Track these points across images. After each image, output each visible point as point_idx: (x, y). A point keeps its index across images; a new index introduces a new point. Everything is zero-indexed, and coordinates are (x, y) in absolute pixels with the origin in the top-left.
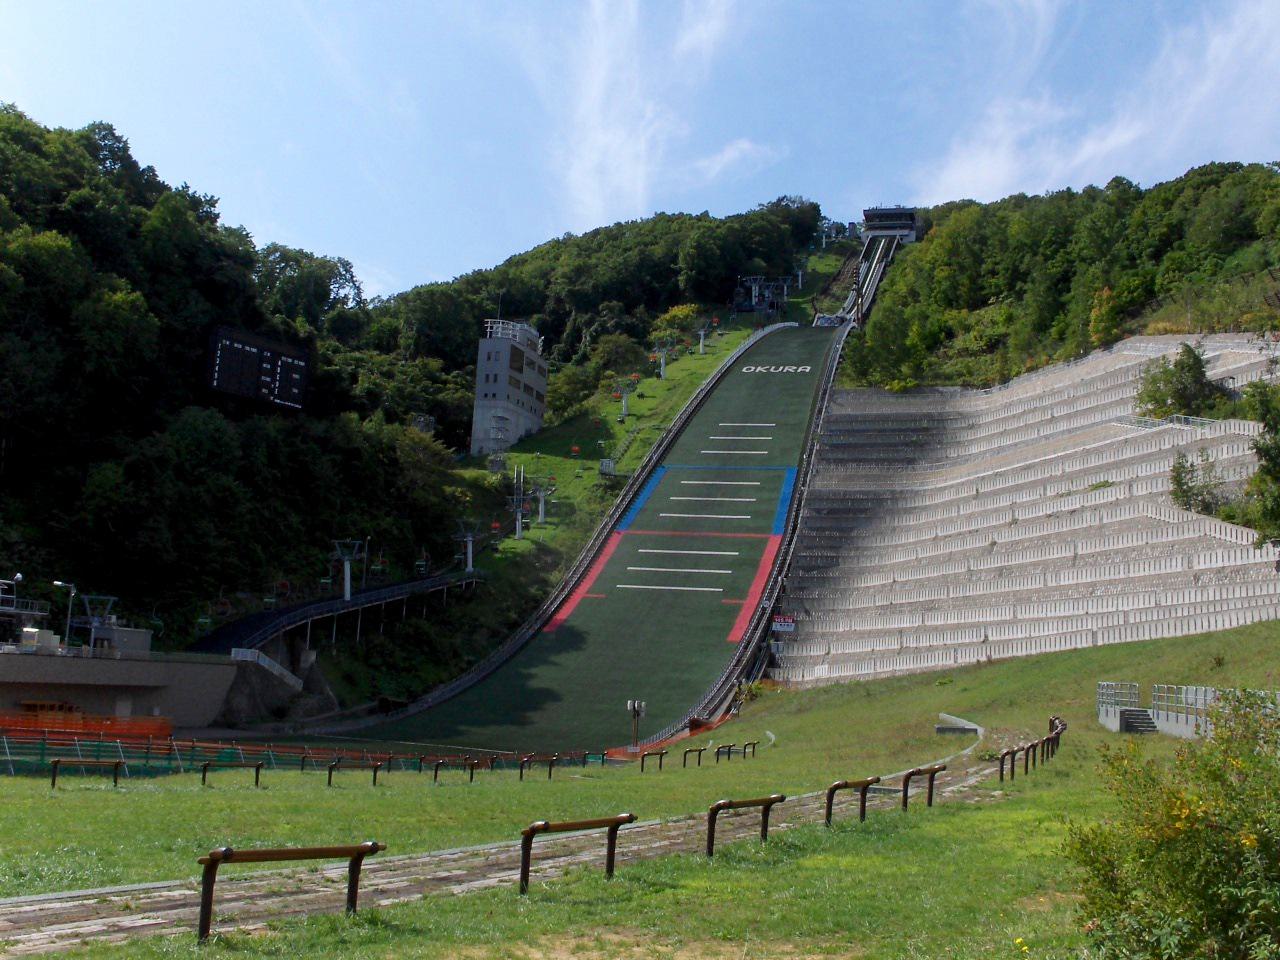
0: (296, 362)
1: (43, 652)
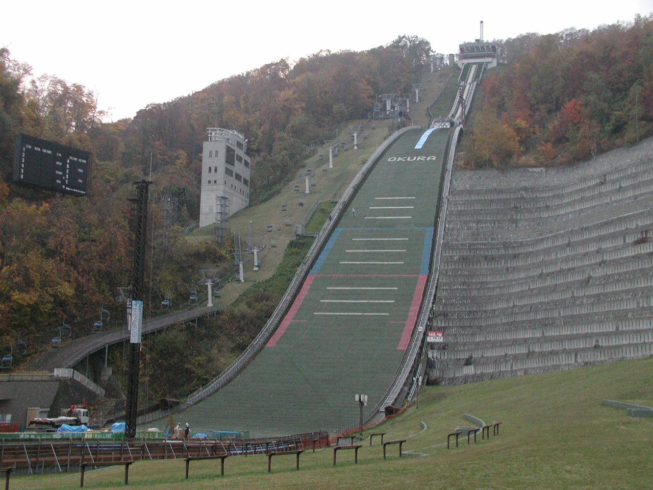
0: (80, 160)
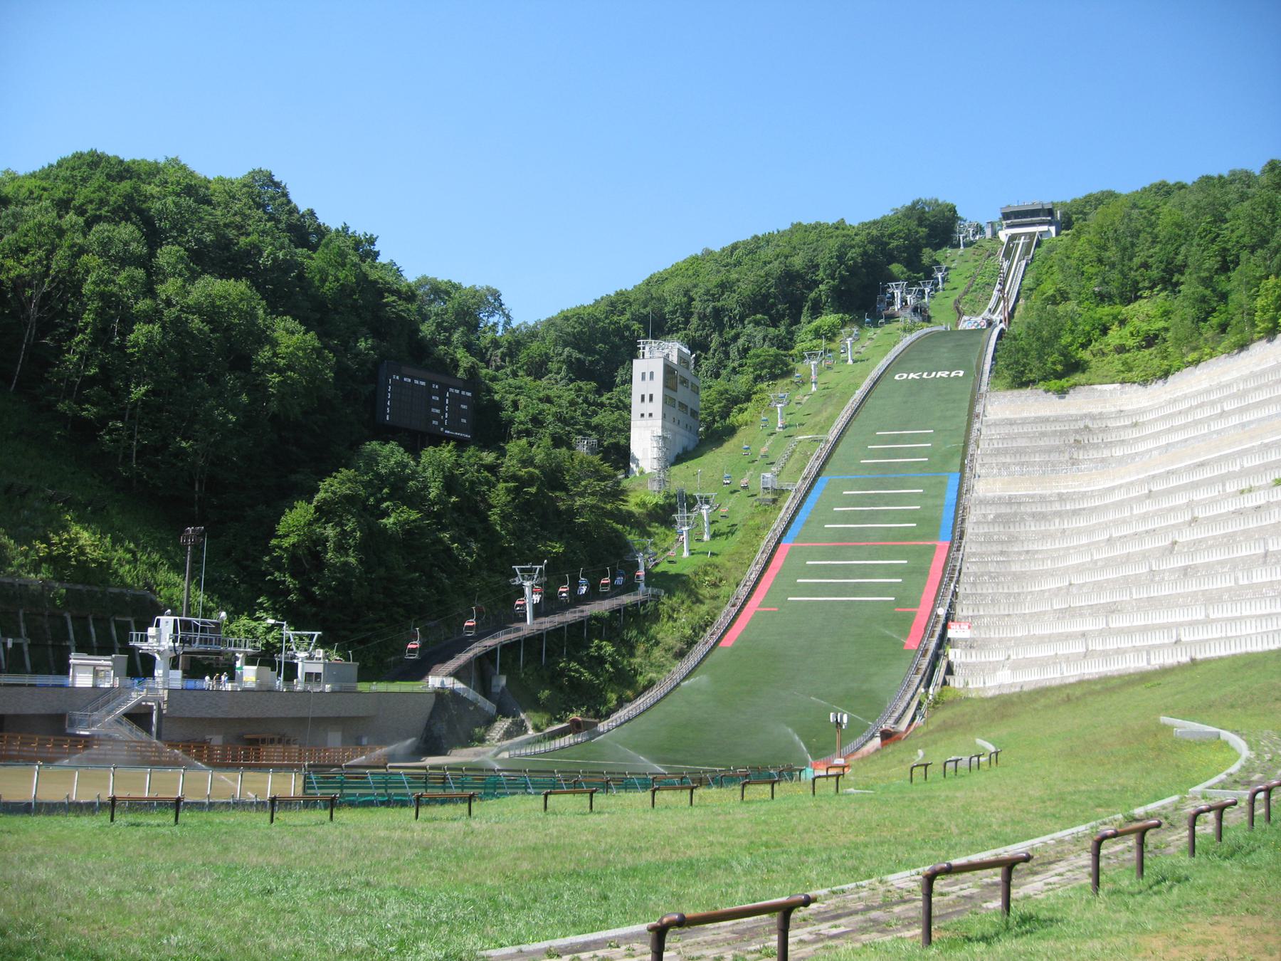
0: (463, 393)
1: (264, 689)
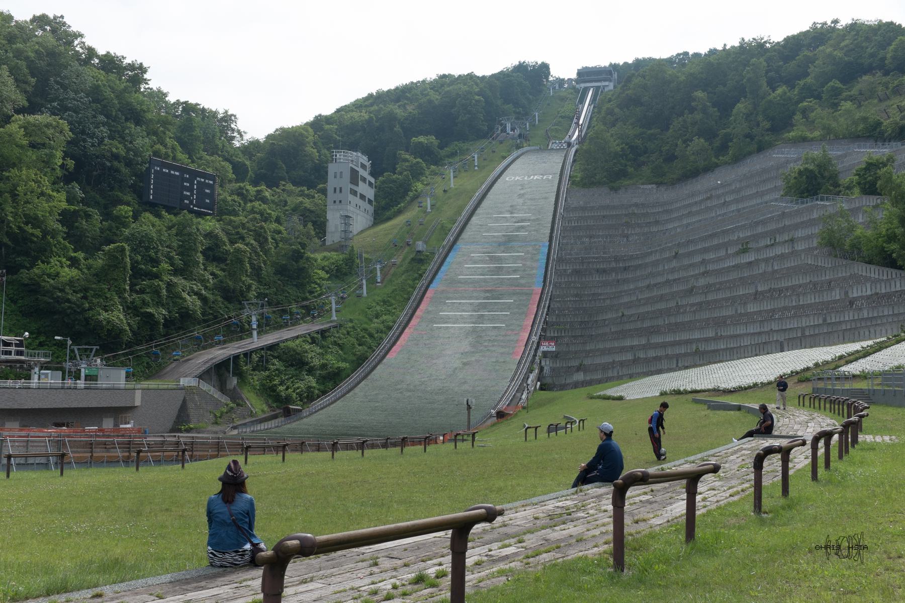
0: (207, 181)
